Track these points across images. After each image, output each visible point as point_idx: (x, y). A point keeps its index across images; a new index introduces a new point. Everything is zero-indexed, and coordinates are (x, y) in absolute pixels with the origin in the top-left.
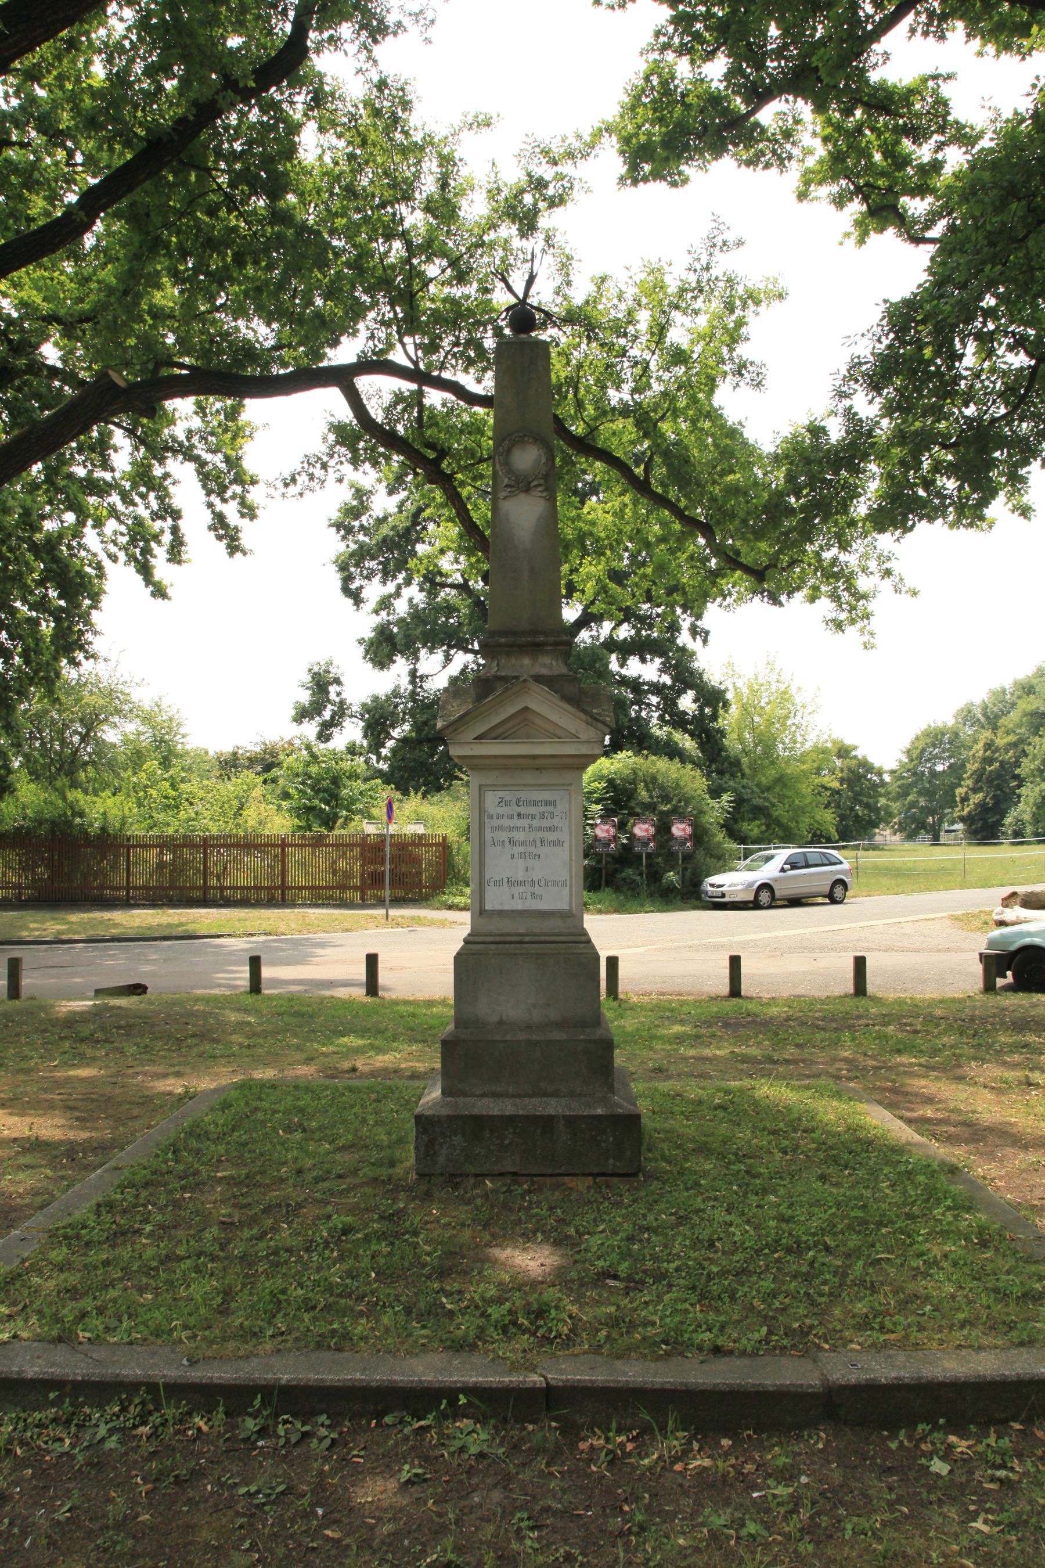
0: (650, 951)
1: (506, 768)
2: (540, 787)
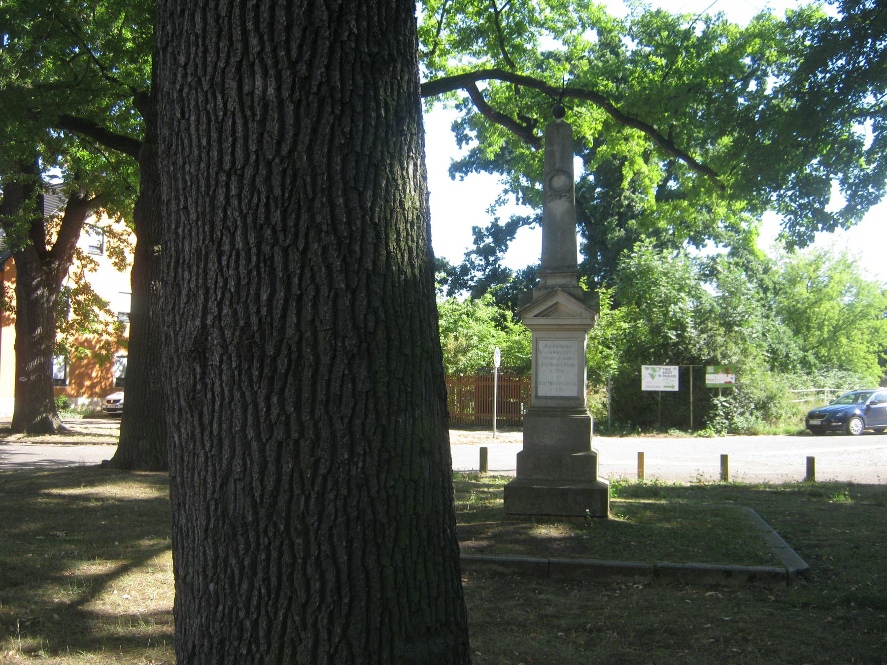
0: (617, 459)
1: (549, 330)
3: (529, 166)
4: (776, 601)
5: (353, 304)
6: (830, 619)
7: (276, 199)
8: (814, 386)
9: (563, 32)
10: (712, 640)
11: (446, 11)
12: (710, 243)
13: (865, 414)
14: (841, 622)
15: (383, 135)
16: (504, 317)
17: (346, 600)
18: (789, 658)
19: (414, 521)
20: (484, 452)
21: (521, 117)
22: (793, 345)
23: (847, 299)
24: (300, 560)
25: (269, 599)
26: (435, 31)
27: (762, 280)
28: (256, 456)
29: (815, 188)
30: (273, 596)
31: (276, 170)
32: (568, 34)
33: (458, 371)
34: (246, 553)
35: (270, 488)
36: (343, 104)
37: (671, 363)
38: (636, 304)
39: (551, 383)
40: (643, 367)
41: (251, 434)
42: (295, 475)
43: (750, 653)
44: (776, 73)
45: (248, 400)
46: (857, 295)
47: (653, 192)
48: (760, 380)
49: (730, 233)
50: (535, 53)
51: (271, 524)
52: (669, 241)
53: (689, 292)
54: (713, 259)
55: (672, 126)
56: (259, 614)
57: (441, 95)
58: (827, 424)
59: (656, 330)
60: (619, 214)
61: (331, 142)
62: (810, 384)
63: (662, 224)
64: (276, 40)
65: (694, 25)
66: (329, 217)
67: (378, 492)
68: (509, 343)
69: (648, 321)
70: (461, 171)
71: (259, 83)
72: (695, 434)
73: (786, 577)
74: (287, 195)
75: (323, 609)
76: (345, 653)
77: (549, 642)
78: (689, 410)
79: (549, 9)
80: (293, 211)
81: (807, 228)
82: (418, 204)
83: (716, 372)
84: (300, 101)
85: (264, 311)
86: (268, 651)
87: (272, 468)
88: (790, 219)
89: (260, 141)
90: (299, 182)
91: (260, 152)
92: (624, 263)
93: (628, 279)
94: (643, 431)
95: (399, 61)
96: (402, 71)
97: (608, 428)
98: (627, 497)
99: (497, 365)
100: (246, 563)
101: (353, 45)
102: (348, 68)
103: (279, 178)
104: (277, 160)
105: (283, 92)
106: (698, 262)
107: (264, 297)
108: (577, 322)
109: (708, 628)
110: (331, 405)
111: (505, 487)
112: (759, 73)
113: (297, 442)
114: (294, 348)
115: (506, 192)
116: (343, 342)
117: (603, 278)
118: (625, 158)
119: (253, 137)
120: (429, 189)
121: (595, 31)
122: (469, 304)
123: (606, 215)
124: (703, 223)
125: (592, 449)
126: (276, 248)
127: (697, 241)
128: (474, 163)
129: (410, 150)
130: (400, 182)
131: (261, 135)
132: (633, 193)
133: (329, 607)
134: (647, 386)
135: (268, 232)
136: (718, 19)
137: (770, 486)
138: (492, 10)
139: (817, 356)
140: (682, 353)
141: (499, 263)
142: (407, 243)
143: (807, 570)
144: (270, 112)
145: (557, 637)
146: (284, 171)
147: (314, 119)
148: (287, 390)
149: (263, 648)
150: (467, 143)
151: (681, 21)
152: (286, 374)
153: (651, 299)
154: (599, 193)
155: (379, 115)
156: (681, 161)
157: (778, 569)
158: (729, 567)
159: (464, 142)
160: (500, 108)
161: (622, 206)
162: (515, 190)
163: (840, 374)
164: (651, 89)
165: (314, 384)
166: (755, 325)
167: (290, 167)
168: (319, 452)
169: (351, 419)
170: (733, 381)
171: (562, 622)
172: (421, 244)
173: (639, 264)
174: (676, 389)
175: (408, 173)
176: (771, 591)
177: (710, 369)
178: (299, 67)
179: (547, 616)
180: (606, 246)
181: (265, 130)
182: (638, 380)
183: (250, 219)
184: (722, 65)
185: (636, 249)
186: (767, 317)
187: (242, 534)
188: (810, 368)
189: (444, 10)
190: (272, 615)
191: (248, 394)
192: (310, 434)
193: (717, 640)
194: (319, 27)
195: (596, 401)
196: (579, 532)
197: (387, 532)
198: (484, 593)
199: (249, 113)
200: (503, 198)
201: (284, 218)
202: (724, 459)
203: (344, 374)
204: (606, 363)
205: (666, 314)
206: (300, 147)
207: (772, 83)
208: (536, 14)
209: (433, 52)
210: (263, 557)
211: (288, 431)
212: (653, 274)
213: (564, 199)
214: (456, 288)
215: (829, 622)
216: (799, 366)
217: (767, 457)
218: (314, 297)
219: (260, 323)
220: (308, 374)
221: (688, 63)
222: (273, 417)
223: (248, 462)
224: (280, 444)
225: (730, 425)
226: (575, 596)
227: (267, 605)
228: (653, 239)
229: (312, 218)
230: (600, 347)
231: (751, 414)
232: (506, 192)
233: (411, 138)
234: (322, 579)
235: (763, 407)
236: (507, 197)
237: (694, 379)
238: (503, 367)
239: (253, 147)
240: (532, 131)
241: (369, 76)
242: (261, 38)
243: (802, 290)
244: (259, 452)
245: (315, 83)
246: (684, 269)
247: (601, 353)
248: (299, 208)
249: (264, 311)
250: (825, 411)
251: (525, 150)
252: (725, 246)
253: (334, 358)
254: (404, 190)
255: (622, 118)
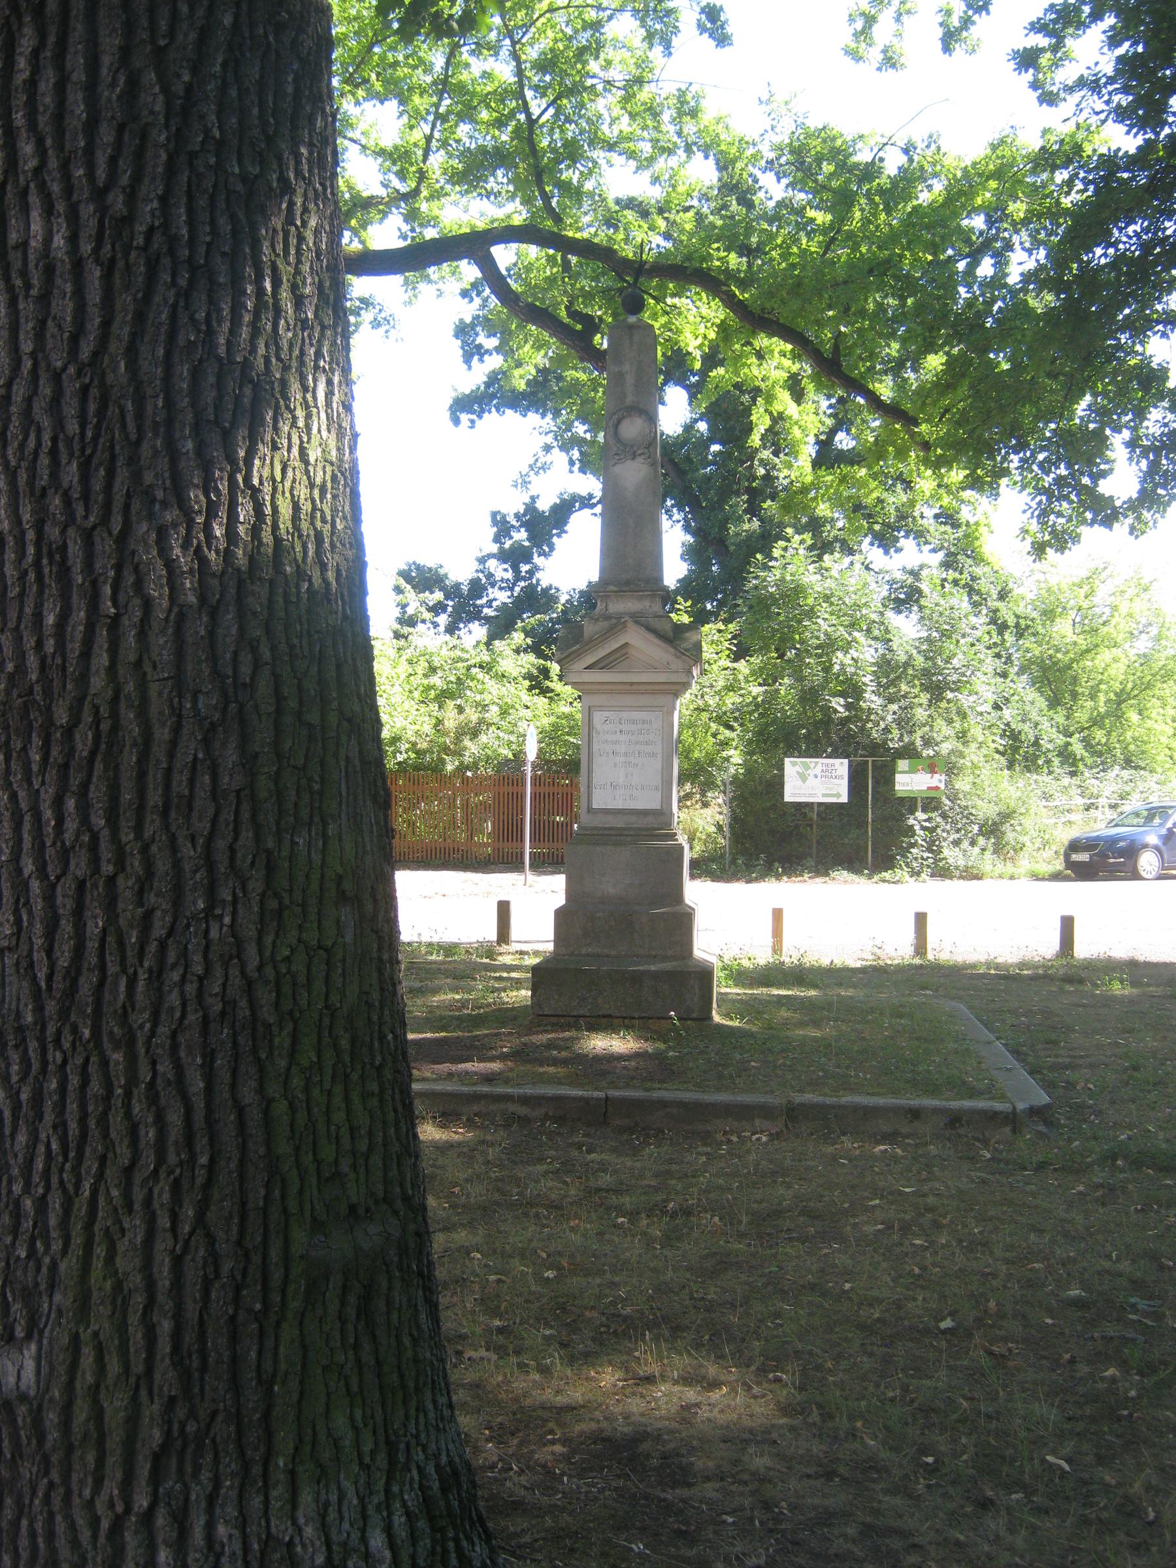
0: (734, 924)
1: (611, 692)
2: (640, 708)
3: (586, 401)
4: (993, 1159)
5: (212, 634)
6: (1081, 1188)
7: (69, 441)
8: (1082, 795)
9: (651, 160)
10: (880, 1227)
11: (444, 118)
12: (908, 544)
13: (1164, 844)
14: (1099, 1193)
15: (269, 327)
16: (545, 672)
17: (204, 1160)
18: (1008, 1254)
19: (326, 1021)
20: (504, 909)
21: (572, 313)
22: (1045, 724)
23: (1143, 645)
24: (120, 1091)
25: (66, 1160)
26: (420, 153)
27: (996, 611)
28: (38, 905)
29: (1084, 450)
30: (72, 1155)
31: (71, 387)
32: (661, 164)
33: (462, 768)
34: (23, 1079)
35: (63, 962)
36: (193, 268)
37: (834, 755)
38: (777, 650)
39: (614, 787)
40: (787, 761)
41: (28, 866)
42: (108, 939)
43: (943, 1246)
44: (1027, 245)
45: (24, 805)
46: (1158, 639)
47: (808, 451)
48: (989, 785)
49: (943, 528)
50: (604, 200)
51: (68, 1026)
52: (836, 539)
53: (869, 631)
54: (915, 574)
55: (839, 335)
56: (48, 1188)
57: (431, 270)
58: (1098, 860)
59: (809, 697)
60: (750, 491)
61: (172, 336)
62: (1075, 791)
63: (823, 509)
64: (68, 146)
65: (881, 154)
66: (167, 475)
67: (260, 968)
68: (553, 719)
69: (797, 680)
70: (472, 412)
71: (36, 226)
72: (876, 878)
73: (1012, 1120)
74: (89, 434)
75: (162, 1175)
76: (201, 1253)
77: (601, 1234)
78: (866, 835)
79: (626, 119)
80: (100, 464)
81: (1070, 520)
82: (334, 453)
83: (912, 770)
84: (113, 260)
85: (50, 646)
86: (64, 1251)
87: (66, 926)
88: (1040, 502)
89: (40, 335)
90: (113, 411)
91: (40, 355)
92: (756, 578)
93: (763, 606)
94: (785, 873)
95: (300, 191)
96: (306, 210)
97: (713, 867)
98: (751, 986)
99: (531, 753)
100: (24, 1097)
101: (212, 161)
102: (202, 202)
103: (75, 403)
104: (72, 370)
105: (82, 244)
106: (887, 578)
107: (50, 619)
108: (662, 678)
109: (875, 1206)
110: (173, 815)
111: (535, 969)
112: (998, 244)
113: (111, 880)
114: (104, 711)
115: (547, 448)
116: (195, 701)
117: (721, 604)
118: (756, 392)
119: (27, 327)
120: (358, 429)
121: (711, 161)
122: (483, 647)
123: (727, 492)
124: (897, 509)
125: (687, 901)
126: (71, 532)
127: (886, 541)
128: (493, 396)
129: (319, 355)
130: (300, 413)
131: (42, 323)
132: (776, 454)
133: (173, 1172)
134: (794, 795)
135: (56, 502)
136: (928, 146)
137: (997, 967)
138: (522, 117)
139: (1087, 743)
140: (854, 737)
141: (538, 575)
142: (312, 523)
143: (1047, 1107)
144: (58, 281)
145: (615, 1226)
146: (85, 389)
147: (140, 295)
148: (92, 788)
149: (56, 1246)
150: (481, 360)
151: (859, 145)
152: (91, 760)
153: (802, 642)
154: (715, 455)
155: (260, 292)
156: (860, 400)
157: (998, 1106)
158: (915, 1102)
159: (476, 358)
160: (534, 295)
161: (754, 478)
162: (565, 447)
163: (1126, 774)
164: (803, 268)
165: (142, 775)
166: (984, 689)
167: (96, 382)
168: (151, 899)
169: (210, 838)
170: (942, 786)
171: (626, 1200)
172: (340, 526)
173: (783, 580)
174: (844, 799)
175: (315, 398)
176: (986, 1142)
177: (902, 764)
178: (110, 198)
179: (598, 1190)
180: (726, 547)
181: (48, 313)
182: (778, 784)
183: (23, 477)
184: (928, 227)
185: (776, 553)
186: (1004, 675)
187: (16, 1047)
188: (1074, 764)
189: (438, 116)
190: (71, 1189)
191: (22, 794)
192: (135, 864)
193: (889, 1227)
194: (147, 124)
195: (701, 821)
196: (662, 1046)
197: (277, 1040)
198: (492, 1153)
199: (18, 282)
200: (542, 460)
201: (85, 478)
202: (921, 920)
203: (195, 758)
204: (724, 754)
205: (827, 669)
206: (113, 347)
207: (1021, 262)
208: (605, 128)
209: (416, 192)
210: (54, 1085)
211: (95, 861)
212: (805, 598)
213: (640, 459)
214: (461, 620)
215: (1080, 1193)
216: (1056, 761)
217: (988, 917)
218: (142, 620)
219: (43, 666)
220: (130, 758)
221: (870, 222)
222: (68, 837)
223: (25, 918)
224: (81, 885)
225: (936, 861)
226: (651, 1156)
227: (61, 1170)
228: (808, 537)
229: (137, 476)
230: (714, 726)
231: (973, 843)
232: (547, 448)
233: (322, 335)
234: (160, 1121)
235: (993, 830)
236: (549, 458)
237: (876, 783)
238: (543, 760)
239: (27, 346)
240: (591, 340)
241: (241, 215)
242: (40, 142)
243: (1064, 630)
244: (44, 899)
245: (140, 228)
246: (850, 587)
247: (714, 735)
248: (113, 458)
249: (50, 646)
250: (1098, 838)
251: (578, 374)
252: (934, 551)
253: (177, 730)
254: (308, 427)
255: (753, 319)
